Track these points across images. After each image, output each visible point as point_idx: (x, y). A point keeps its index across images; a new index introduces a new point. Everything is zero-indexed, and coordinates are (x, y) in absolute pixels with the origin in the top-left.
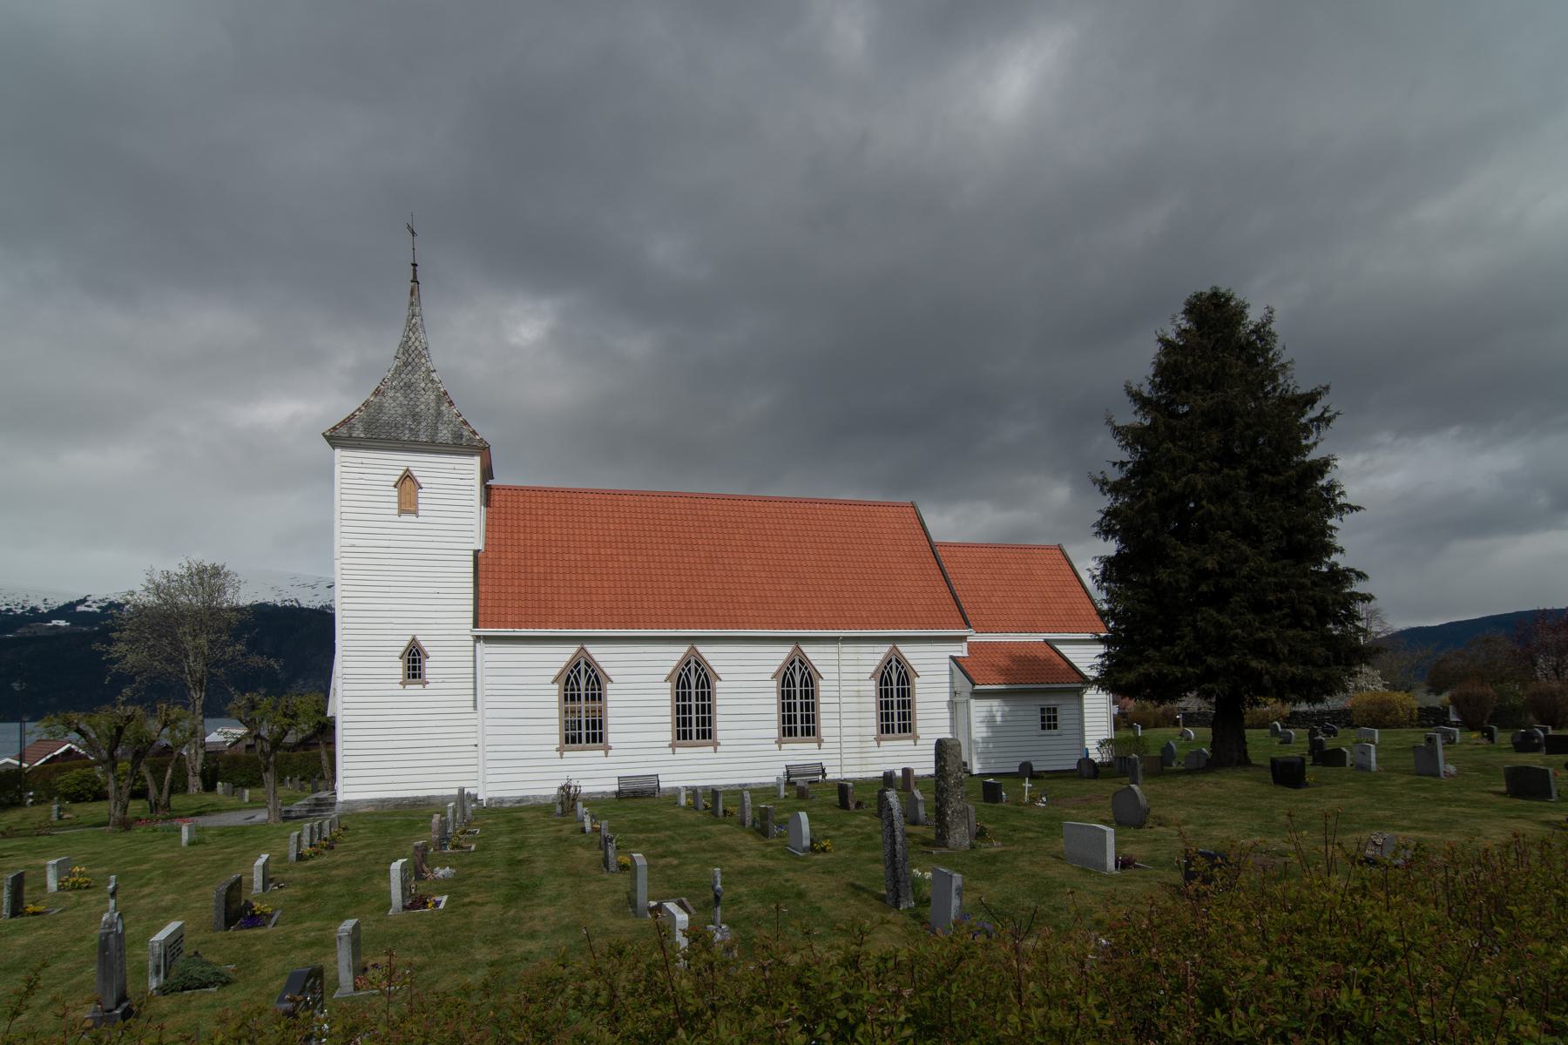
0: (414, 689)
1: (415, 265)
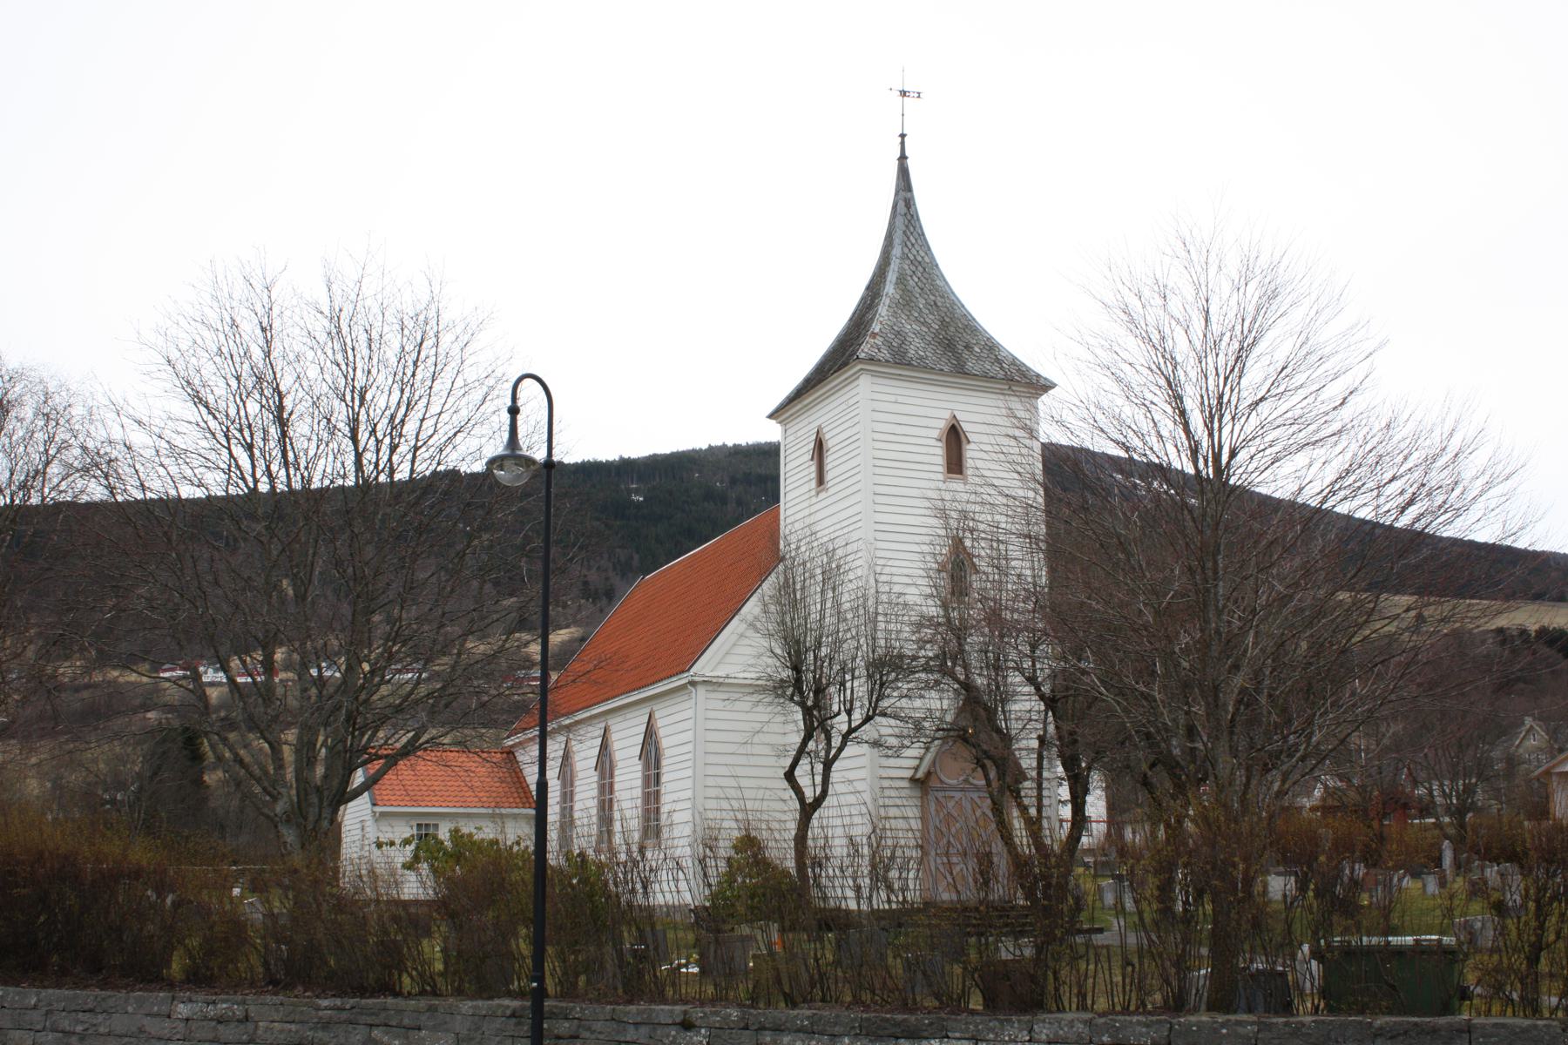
1: (903, 136)
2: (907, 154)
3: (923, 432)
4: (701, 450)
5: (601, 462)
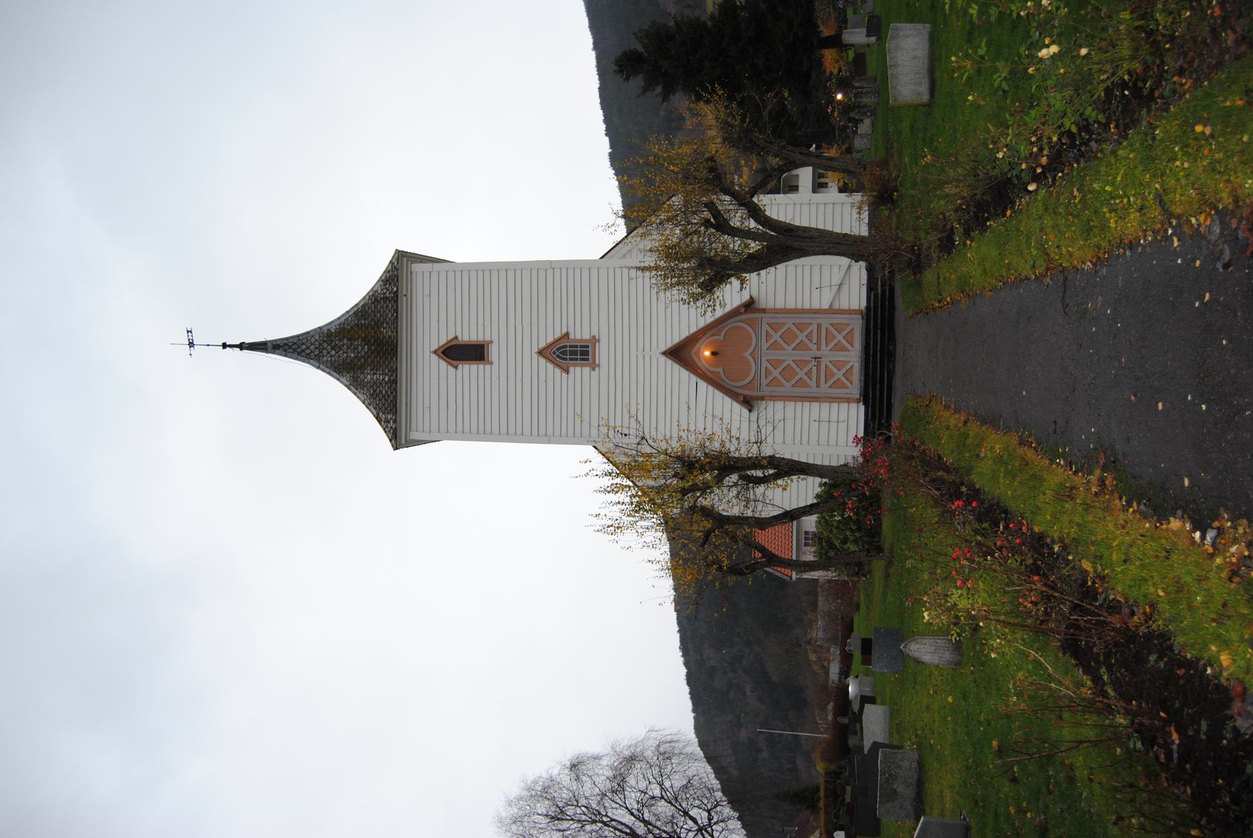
1: (225, 346)
2: (238, 343)
3: (451, 382)
5: (607, 130)
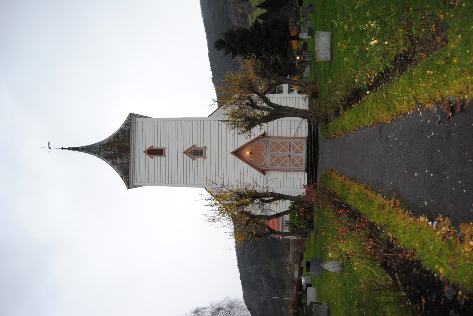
0: (167, 152)
1: (63, 148)
4: (203, 19)
